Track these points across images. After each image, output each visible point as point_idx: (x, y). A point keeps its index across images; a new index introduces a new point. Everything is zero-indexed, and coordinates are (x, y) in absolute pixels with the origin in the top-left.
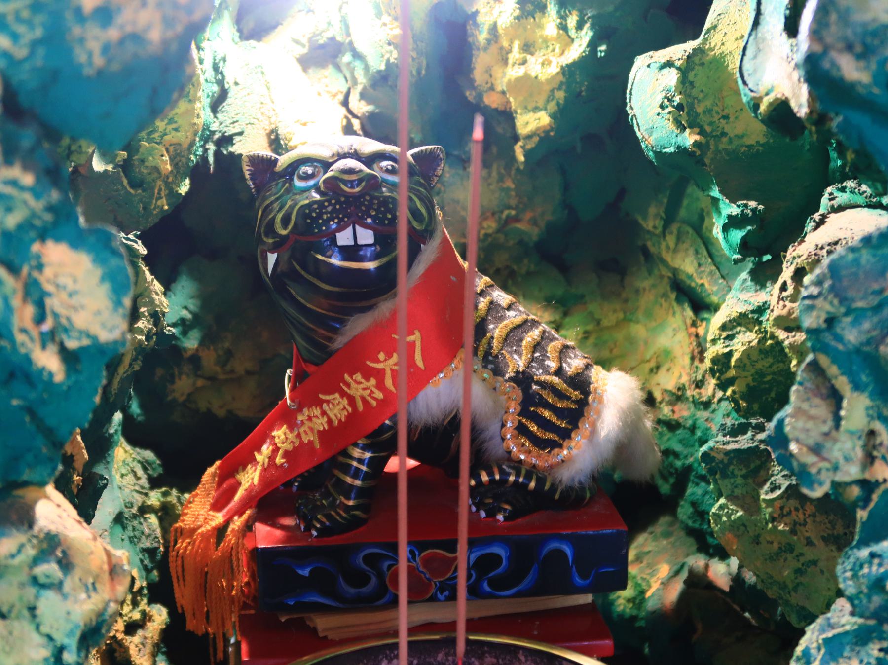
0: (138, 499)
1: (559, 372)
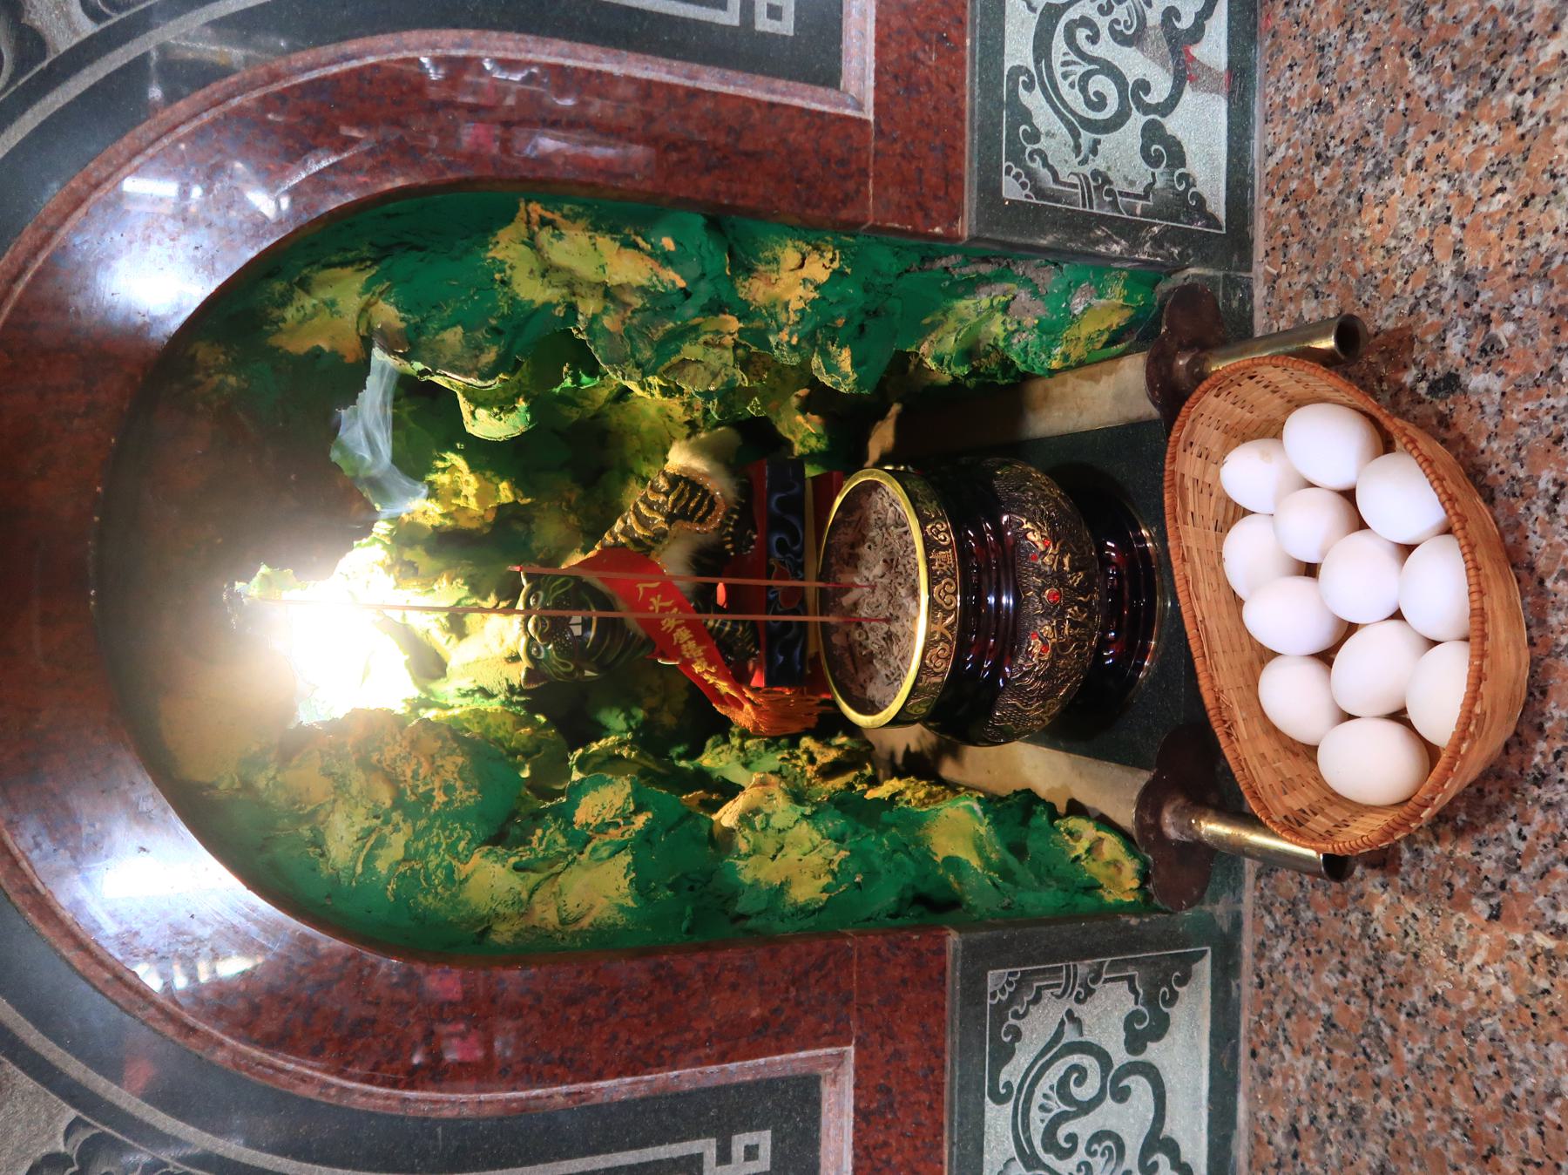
0: (735, 752)
1: (667, 494)
